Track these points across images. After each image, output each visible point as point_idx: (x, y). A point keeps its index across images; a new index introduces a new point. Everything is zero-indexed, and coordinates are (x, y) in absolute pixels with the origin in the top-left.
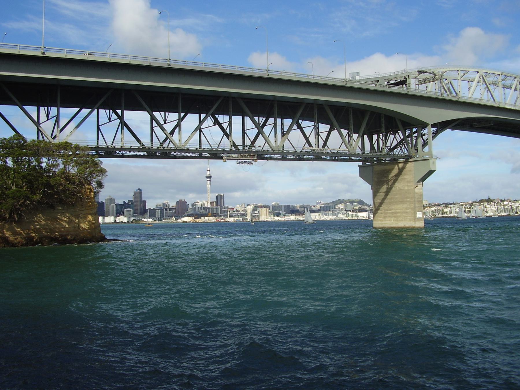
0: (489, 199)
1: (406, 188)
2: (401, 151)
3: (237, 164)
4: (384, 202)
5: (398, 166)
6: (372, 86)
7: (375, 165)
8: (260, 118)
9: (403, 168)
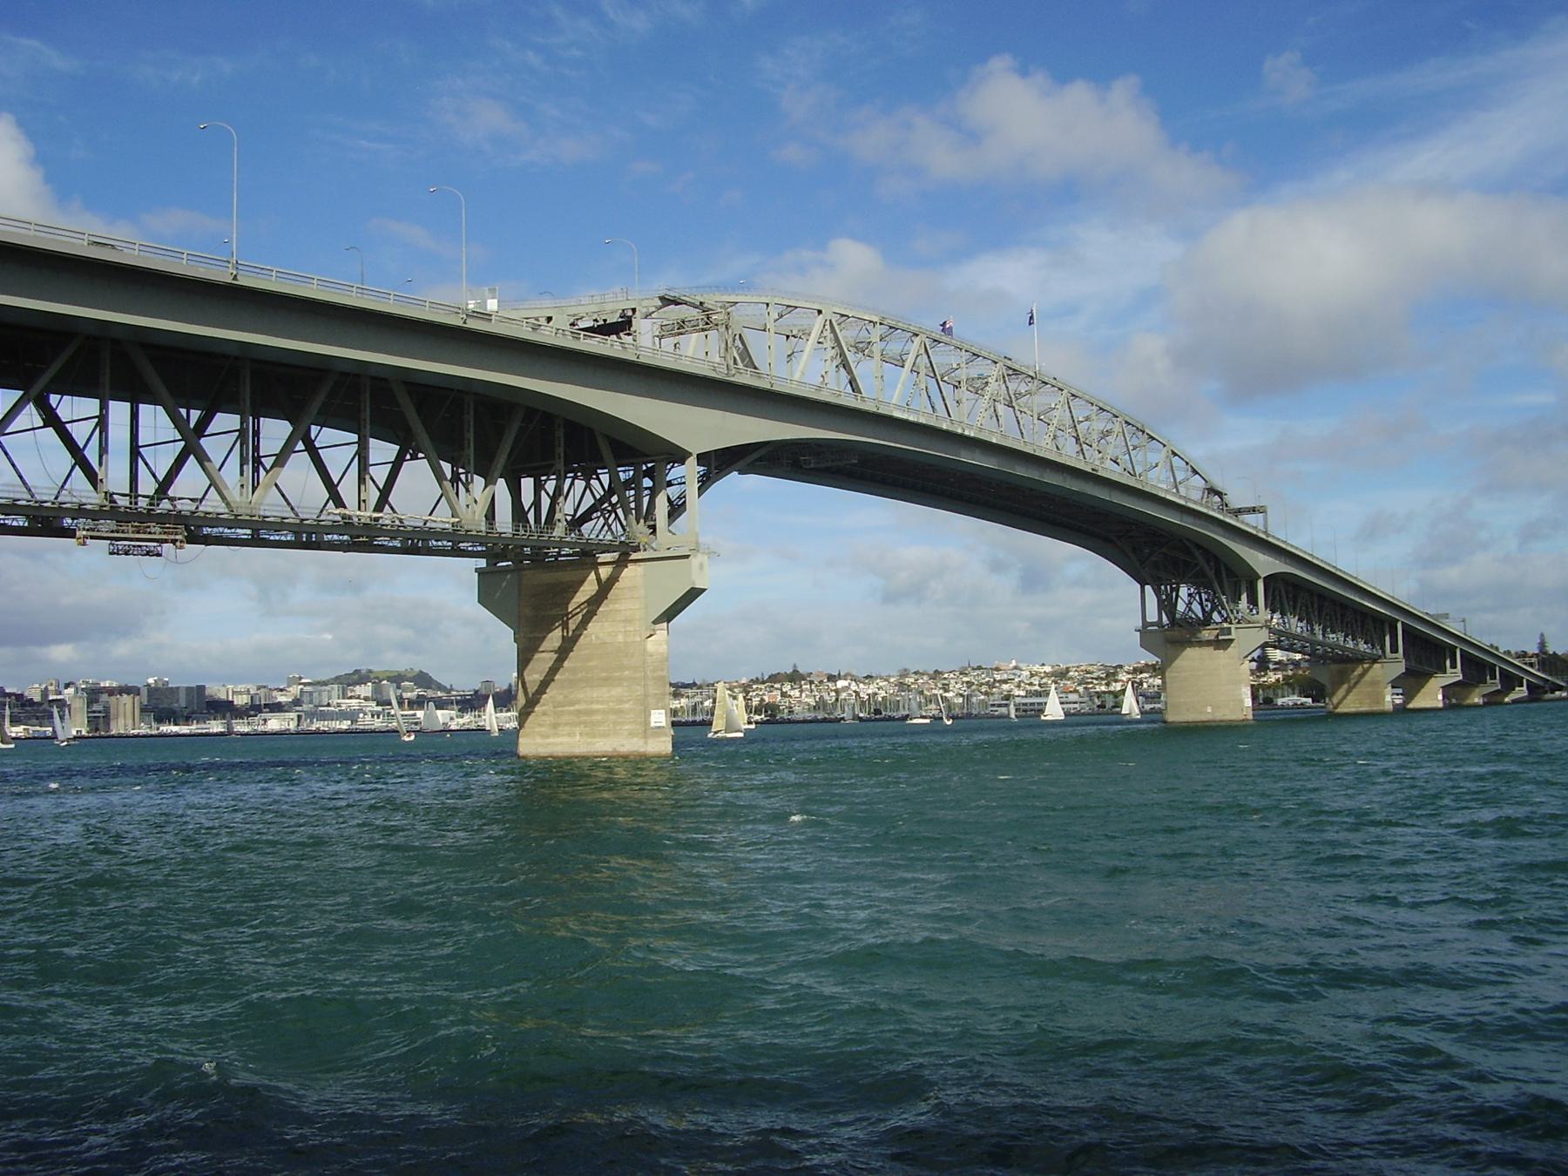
0: (795, 671)
1: (620, 638)
2: (606, 528)
3: (110, 553)
4: (553, 680)
5: (598, 575)
7: (524, 569)
8: (192, 411)
9: (613, 579)
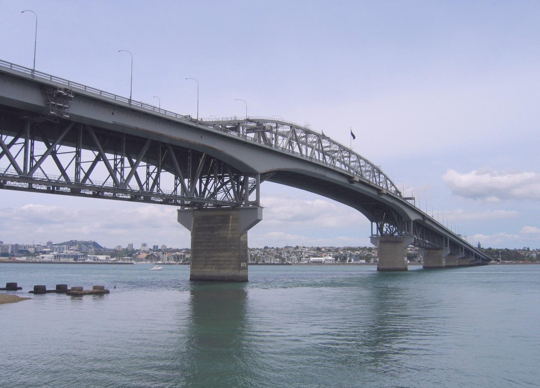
6: (211, 128)
